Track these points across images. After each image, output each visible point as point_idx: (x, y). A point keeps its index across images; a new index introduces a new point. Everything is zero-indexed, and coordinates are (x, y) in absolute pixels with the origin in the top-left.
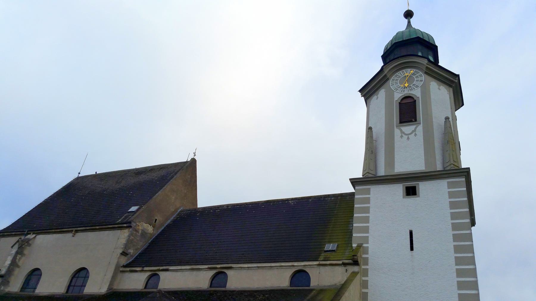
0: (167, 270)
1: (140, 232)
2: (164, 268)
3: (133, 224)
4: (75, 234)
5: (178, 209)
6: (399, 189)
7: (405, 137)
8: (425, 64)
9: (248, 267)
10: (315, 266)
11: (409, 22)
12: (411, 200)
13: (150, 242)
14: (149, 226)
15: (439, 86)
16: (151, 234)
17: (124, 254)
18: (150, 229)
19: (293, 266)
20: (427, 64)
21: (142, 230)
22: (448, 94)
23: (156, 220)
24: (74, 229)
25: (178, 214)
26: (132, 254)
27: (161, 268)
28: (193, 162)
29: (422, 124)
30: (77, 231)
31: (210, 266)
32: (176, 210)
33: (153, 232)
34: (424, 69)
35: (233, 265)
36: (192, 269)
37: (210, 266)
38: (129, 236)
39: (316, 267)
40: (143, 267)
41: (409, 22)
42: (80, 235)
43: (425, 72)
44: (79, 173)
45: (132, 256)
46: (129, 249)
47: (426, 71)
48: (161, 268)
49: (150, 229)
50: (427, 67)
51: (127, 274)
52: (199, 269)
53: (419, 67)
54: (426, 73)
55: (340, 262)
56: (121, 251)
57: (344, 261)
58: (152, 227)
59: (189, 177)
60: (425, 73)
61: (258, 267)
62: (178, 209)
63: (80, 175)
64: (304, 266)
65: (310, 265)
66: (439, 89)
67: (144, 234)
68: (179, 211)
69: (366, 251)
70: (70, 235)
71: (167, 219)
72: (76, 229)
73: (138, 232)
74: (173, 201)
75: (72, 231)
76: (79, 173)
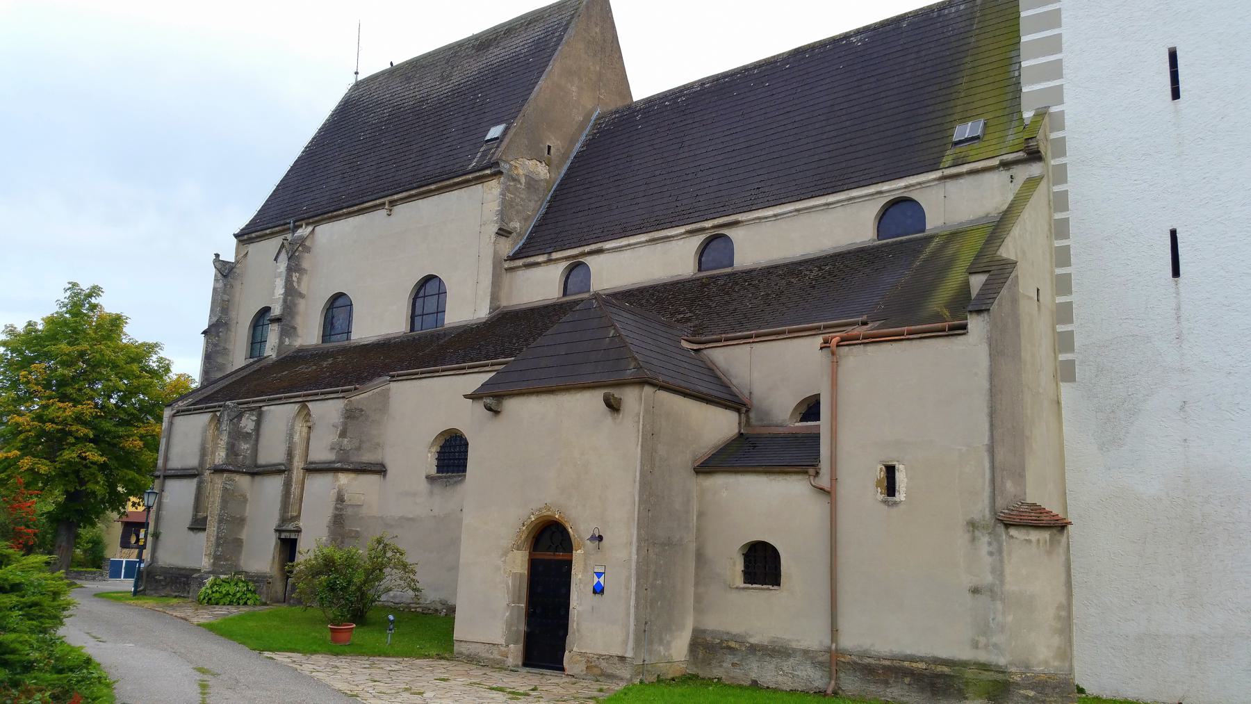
1: (523, 180)
3: (504, 167)
4: (391, 210)
9: (775, 216)
17: (503, 233)
19: (881, 192)
21: (526, 176)
23: (549, 148)
24: (386, 200)
30: (393, 203)
32: (587, 116)
35: (740, 217)
40: (550, 253)
42: (400, 209)
46: (511, 220)
48: (587, 249)
57: (1004, 157)
63: (360, 77)
64: (906, 187)
70: (383, 213)
73: (519, 182)
74: (574, 98)
75: (384, 204)
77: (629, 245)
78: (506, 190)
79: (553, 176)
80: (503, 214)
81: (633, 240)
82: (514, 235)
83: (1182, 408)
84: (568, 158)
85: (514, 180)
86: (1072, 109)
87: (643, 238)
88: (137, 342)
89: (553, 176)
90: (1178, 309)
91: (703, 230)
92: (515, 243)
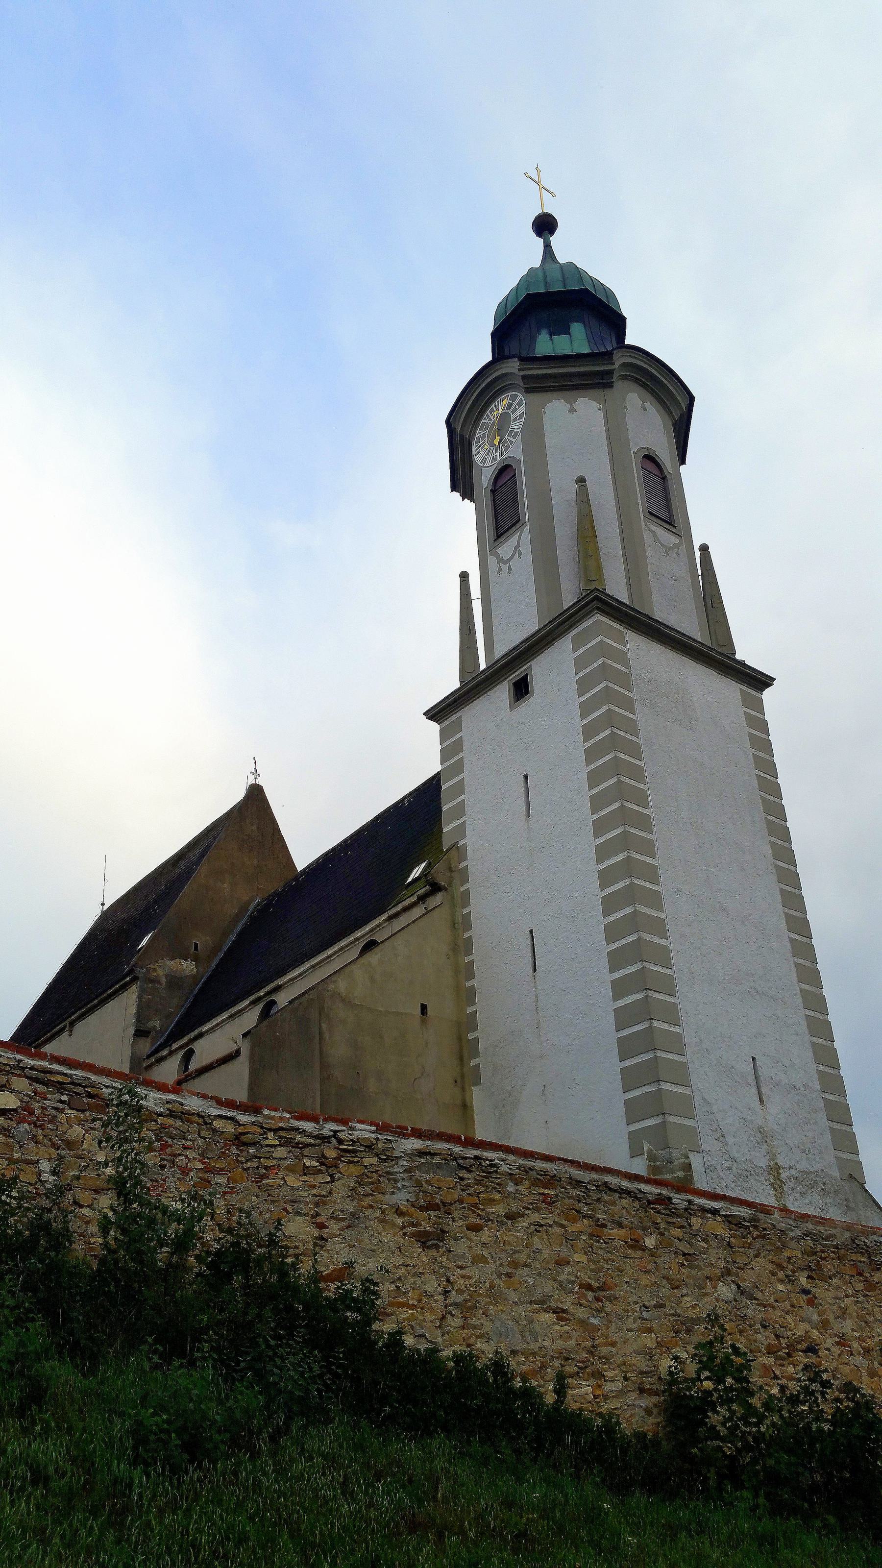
0: (200, 1036)
1: (164, 980)
2: (196, 1032)
3: (140, 972)
4: (72, 1031)
5: (249, 903)
6: (502, 692)
7: (505, 567)
8: (516, 371)
9: (300, 975)
10: (385, 925)
11: (548, 247)
12: (530, 704)
13: (195, 992)
14: (182, 961)
15: (571, 402)
16: (193, 976)
17: (140, 1033)
18: (188, 967)
19: (357, 939)
20: (519, 370)
21: (166, 976)
22: (600, 409)
23: (196, 945)
24: (67, 1022)
25: (250, 916)
26: (159, 1028)
27: (192, 1035)
28: (256, 795)
29: (527, 523)
30: (72, 1024)
31: (252, 998)
32: (243, 909)
33: (197, 971)
34: (521, 384)
35: (280, 981)
36: (231, 1017)
37: (252, 998)
38: (140, 997)
39: (388, 925)
40: (170, 1046)
41: (548, 247)
42: (79, 1027)
43: (526, 388)
44: (103, 904)
45: (160, 1033)
46: (149, 1020)
47: (526, 386)
48: (192, 1035)
49: (188, 967)
50: (524, 377)
51: (155, 1068)
52: (240, 1011)
53: (513, 384)
54: (528, 391)
55: (414, 899)
56: (132, 1031)
57: (419, 893)
58: (190, 961)
59: (254, 827)
60: (526, 392)
61: (313, 967)
62: (249, 903)
63: (105, 908)
64: (371, 931)
65: (377, 926)
66: (572, 410)
67: (175, 981)
68: (251, 908)
69: (463, 856)
70: (66, 1034)
71: (225, 935)
72: (69, 1020)
73: (159, 983)
74: (226, 894)
75: (65, 1027)
76: (103, 904)
77: (218, 1024)
78: (142, 992)
79: (201, 970)
80: (139, 1017)
81: (219, 1019)
82: (153, 1033)
83: (543, 1093)
84: (220, 950)
85: (152, 981)
86: (470, 841)
87: (225, 1016)
88: (876, 1456)
89: (201, 970)
90: (537, 996)
91: (259, 999)
92: (152, 1044)
